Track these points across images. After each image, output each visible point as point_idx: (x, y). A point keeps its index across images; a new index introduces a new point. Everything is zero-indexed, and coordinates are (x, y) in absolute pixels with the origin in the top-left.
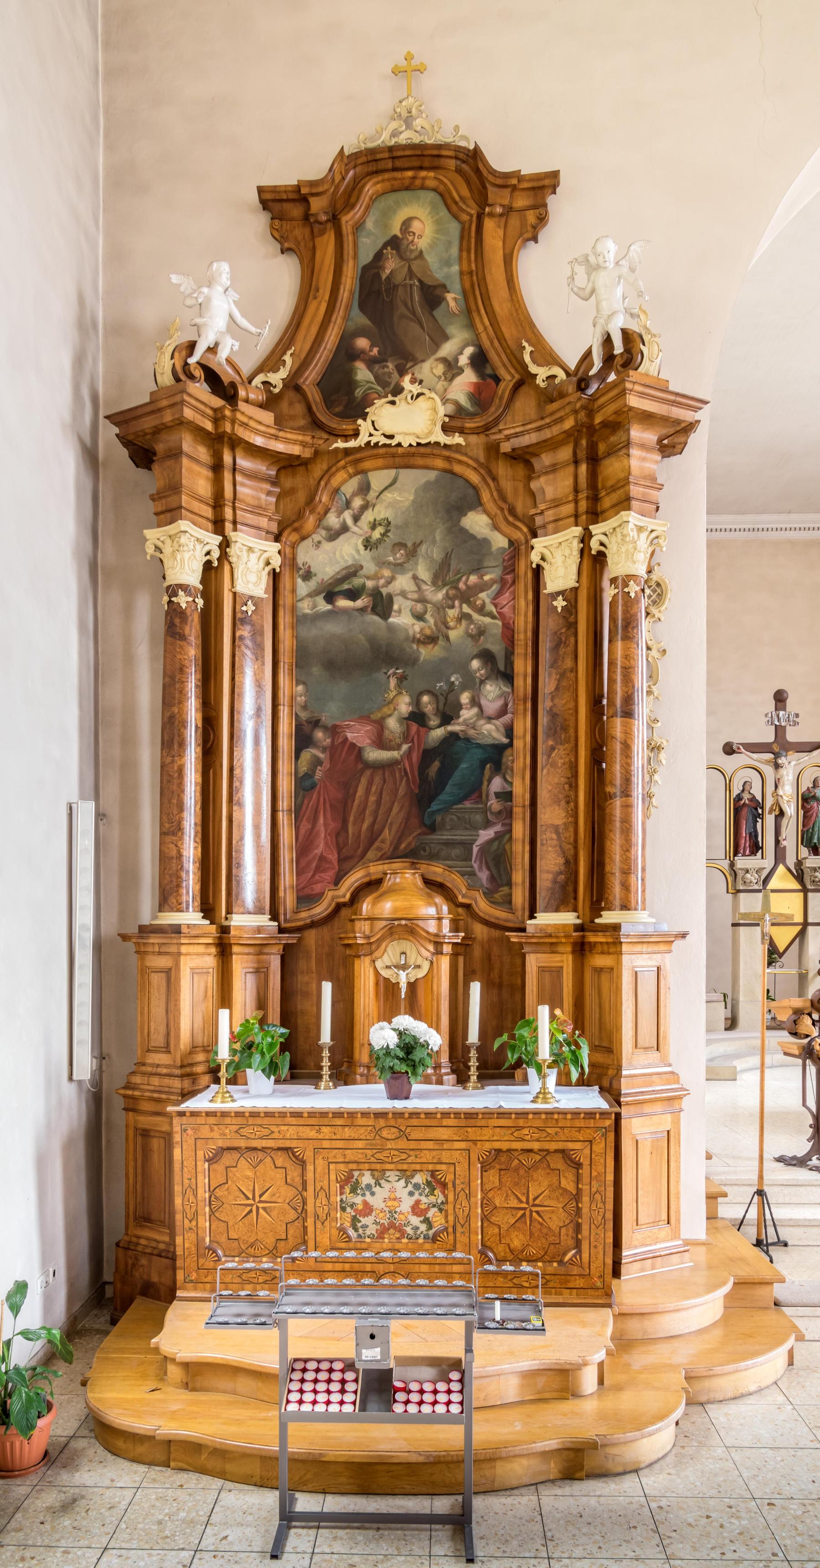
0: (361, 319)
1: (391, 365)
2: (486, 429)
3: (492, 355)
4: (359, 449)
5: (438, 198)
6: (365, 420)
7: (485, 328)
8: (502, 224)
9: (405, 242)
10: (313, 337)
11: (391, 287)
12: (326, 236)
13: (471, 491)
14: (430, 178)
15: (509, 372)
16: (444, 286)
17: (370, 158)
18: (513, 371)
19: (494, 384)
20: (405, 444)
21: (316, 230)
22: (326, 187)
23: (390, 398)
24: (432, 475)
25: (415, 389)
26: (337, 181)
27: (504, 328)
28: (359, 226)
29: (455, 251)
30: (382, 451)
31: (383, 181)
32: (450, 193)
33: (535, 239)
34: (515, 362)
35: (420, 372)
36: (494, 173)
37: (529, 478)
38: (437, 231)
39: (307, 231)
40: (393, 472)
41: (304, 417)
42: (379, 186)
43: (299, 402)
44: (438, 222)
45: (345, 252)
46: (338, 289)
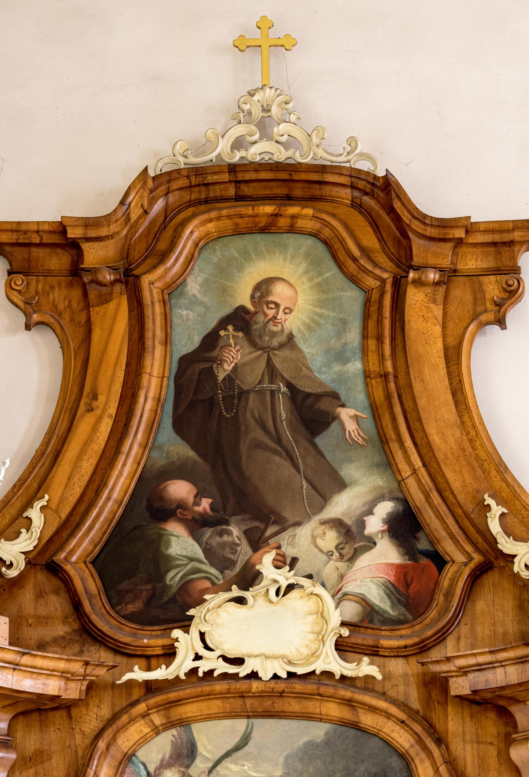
0: (176, 447)
1: (235, 531)
2: (423, 648)
3: (428, 517)
4: (175, 683)
5: (321, 247)
6: (186, 629)
7: (414, 471)
8: (440, 296)
9: (260, 318)
10: (87, 478)
11: (235, 392)
12: (111, 306)
13: (395, 762)
14: (305, 217)
15: (462, 550)
16: (335, 396)
17: (194, 181)
18: (469, 548)
19: (433, 568)
20: (266, 675)
21: (92, 295)
22: (113, 228)
23: (236, 592)
24: (318, 731)
25: (284, 577)
26: (134, 217)
27: (449, 475)
28: (173, 290)
29: (353, 336)
30: (220, 687)
31: (218, 218)
32: (342, 242)
33: (501, 322)
34: (471, 530)
35: (291, 544)
36: (422, 218)
37: (508, 741)
38: (321, 304)
39: (76, 293)
40: (241, 724)
41: (65, 620)
42: (211, 226)
43: (56, 592)
44: (322, 288)
45: (149, 335)
46: (134, 396)
